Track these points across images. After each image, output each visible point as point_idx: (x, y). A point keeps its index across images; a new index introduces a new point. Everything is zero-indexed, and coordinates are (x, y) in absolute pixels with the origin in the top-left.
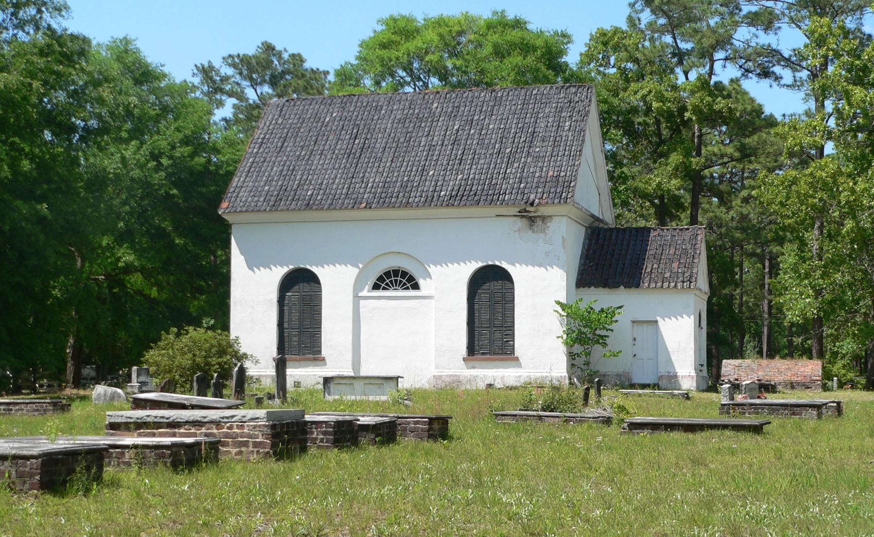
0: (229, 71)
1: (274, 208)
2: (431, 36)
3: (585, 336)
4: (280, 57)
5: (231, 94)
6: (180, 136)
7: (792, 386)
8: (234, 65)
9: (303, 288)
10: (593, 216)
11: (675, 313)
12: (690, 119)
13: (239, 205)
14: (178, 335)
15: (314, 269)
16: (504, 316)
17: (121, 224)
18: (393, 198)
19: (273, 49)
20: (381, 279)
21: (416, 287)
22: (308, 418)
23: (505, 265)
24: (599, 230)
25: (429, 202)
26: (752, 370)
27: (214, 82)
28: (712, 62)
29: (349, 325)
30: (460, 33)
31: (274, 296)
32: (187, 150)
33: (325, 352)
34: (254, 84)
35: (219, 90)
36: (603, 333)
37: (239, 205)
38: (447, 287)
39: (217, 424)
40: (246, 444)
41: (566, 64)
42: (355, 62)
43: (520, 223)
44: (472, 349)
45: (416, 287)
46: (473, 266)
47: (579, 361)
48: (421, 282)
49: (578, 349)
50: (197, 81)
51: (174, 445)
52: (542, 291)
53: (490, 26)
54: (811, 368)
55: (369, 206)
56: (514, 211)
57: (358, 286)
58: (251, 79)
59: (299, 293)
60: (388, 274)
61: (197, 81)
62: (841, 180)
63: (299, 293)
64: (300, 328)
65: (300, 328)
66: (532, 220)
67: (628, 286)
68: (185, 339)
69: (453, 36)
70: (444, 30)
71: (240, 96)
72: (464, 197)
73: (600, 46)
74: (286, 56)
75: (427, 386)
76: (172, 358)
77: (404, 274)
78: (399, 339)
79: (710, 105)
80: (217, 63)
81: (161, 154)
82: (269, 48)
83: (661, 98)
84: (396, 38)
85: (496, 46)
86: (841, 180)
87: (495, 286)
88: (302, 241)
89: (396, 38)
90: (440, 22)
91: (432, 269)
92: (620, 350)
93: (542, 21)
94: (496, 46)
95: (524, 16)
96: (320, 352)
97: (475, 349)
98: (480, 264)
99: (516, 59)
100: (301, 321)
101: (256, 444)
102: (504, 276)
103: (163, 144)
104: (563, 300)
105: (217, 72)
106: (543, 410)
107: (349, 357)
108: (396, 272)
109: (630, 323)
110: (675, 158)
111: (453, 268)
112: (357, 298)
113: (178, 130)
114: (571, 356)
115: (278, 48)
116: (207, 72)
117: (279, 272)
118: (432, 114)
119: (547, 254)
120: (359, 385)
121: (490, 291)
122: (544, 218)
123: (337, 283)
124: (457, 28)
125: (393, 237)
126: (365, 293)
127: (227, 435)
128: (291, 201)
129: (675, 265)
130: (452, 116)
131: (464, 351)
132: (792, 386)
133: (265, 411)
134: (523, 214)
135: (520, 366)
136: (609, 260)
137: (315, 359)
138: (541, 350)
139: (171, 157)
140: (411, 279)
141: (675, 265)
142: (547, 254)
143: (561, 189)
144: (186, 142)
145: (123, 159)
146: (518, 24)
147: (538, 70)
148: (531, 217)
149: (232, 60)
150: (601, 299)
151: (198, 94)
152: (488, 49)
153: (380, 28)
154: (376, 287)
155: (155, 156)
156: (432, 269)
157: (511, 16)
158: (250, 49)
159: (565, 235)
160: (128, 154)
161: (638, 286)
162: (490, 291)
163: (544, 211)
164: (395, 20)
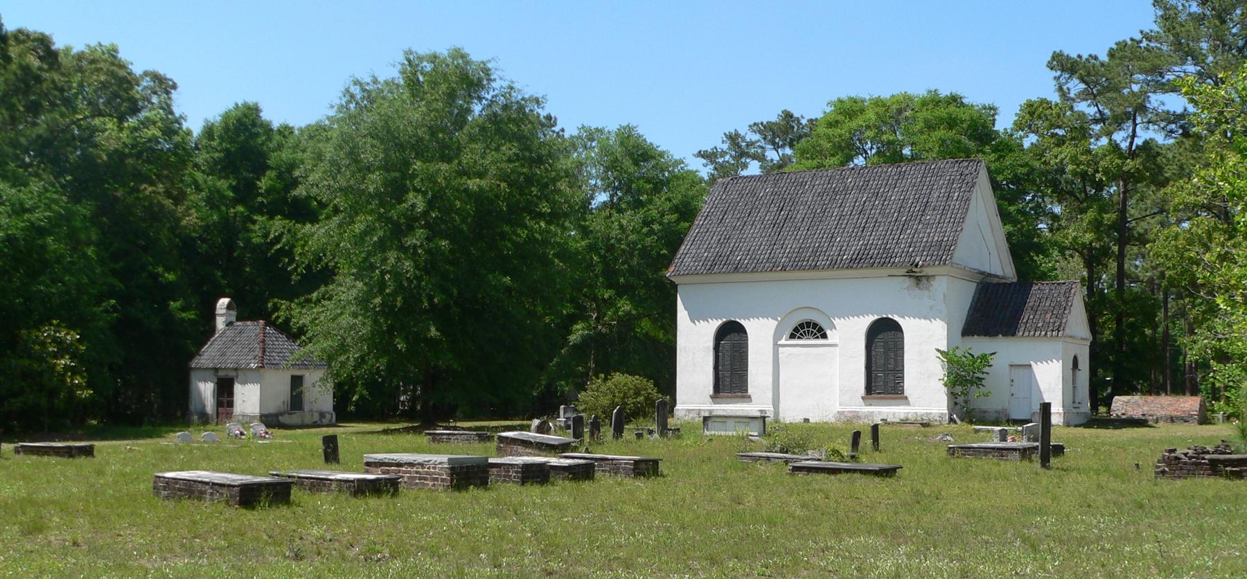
0: (755, 137)
1: (710, 271)
2: (871, 115)
3: (963, 378)
4: (799, 123)
5: (754, 157)
6: (668, 205)
7: (1172, 420)
8: (760, 132)
9: (734, 337)
10: (982, 273)
11: (1046, 359)
12: (1101, 180)
13: (682, 269)
14: (605, 380)
15: (742, 322)
16: (896, 361)
17: (622, 280)
18: (808, 262)
19: (791, 116)
20: (796, 330)
21: (824, 336)
22: (491, 461)
23: (896, 318)
24: (989, 284)
25: (833, 265)
26: (1139, 406)
27: (740, 147)
28: (1135, 125)
29: (770, 368)
30: (900, 111)
31: (710, 343)
32: (674, 217)
33: (751, 391)
34: (776, 147)
35: (743, 154)
36: (980, 375)
37: (682, 269)
38: (849, 334)
39: (422, 465)
40: (436, 479)
41: (997, 132)
42: (1104, 58)
43: (908, 282)
44: (869, 389)
45: (824, 336)
46: (870, 319)
47: (960, 400)
48: (828, 332)
49: (959, 389)
50: (725, 147)
51: (359, 480)
52: (927, 341)
53: (924, 103)
54: (1190, 404)
55: (784, 269)
56: (903, 271)
57: (777, 336)
58: (773, 143)
59: (730, 340)
60: (802, 325)
61: (725, 147)
62: (1215, 235)
63: (730, 340)
64: (730, 373)
65: (730, 373)
66: (918, 279)
67: (1005, 335)
68: (609, 383)
69: (894, 113)
70: (881, 110)
71: (761, 158)
72: (860, 261)
73: (1027, 116)
74: (804, 122)
75: (833, 420)
76: (596, 398)
77: (815, 325)
78: (813, 383)
79: (1119, 167)
80: (743, 130)
81: (652, 222)
82: (788, 116)
83: (1074, 160)
84: (840, 118)
85: (926, 121)
86: (1215, 235)
87: (888, 336)
88: (732, 299)
89: (840, 118)
90: (878, 102)
91: (837, 321)
92: (995, 392)
93: (975, 97)
94: (926, 121)
95: (959, 91)
96: (746, 391)
97: (871, 389)
98: (877, 317)
99: (941, 133)
100: (732, 365)
101: (443, 480)
102: (896, 328)
103: (654, 213)
104: (944, 348)
105: (743, 139)
106: (781, 452)
107: (770, 395)
108: (808, 324)
109: (1007, 368)
110: (1091, 214)
111: (854, 320)
112: (776, 346)
113: (669, 200)
114: (952, 395)
115: (796, 115)
116: (733, 138)
117: (715, 324)
118: (846, 189)
119: (931, 308)
120: (730, 423)
121: (884, 341)
122: (928, 277)
123: (760, 334)
124: (894, 107)
125: (806, 295)
126: (783, 342)
127: (427, 473)
128: (725, 266)
129: (1048, 316)
130: (861, 190)
131: (862, 391)
132: (1172, 420)
133: (444, 458)
134: (910, 274)
135: (908, 404)
136: (995, 311)
137: (743, 397)
138: (926, 391)
139: (661, 224)
140: (821, 330)
141: (1048, 316)
142: (931, 308)
143: (942, 252)
144: (675, 209)
145: (621, 226)
146: (954, 100)
147: (959, 142)
148: (917, 277)
149: (755, 127)
150: (980, 345)
151: (727, 158)
152: (920, 125)
153: (829, 109)
154: (792, 336)
155: (646, 223)
156: (837, 321)
157: (944, 92)
158: (773, 116)
159: (953, 293)
160: (624, 222)
161: (1014, 334)
162: (884, 341)
163: (928, 271)
164: (841, 101)
